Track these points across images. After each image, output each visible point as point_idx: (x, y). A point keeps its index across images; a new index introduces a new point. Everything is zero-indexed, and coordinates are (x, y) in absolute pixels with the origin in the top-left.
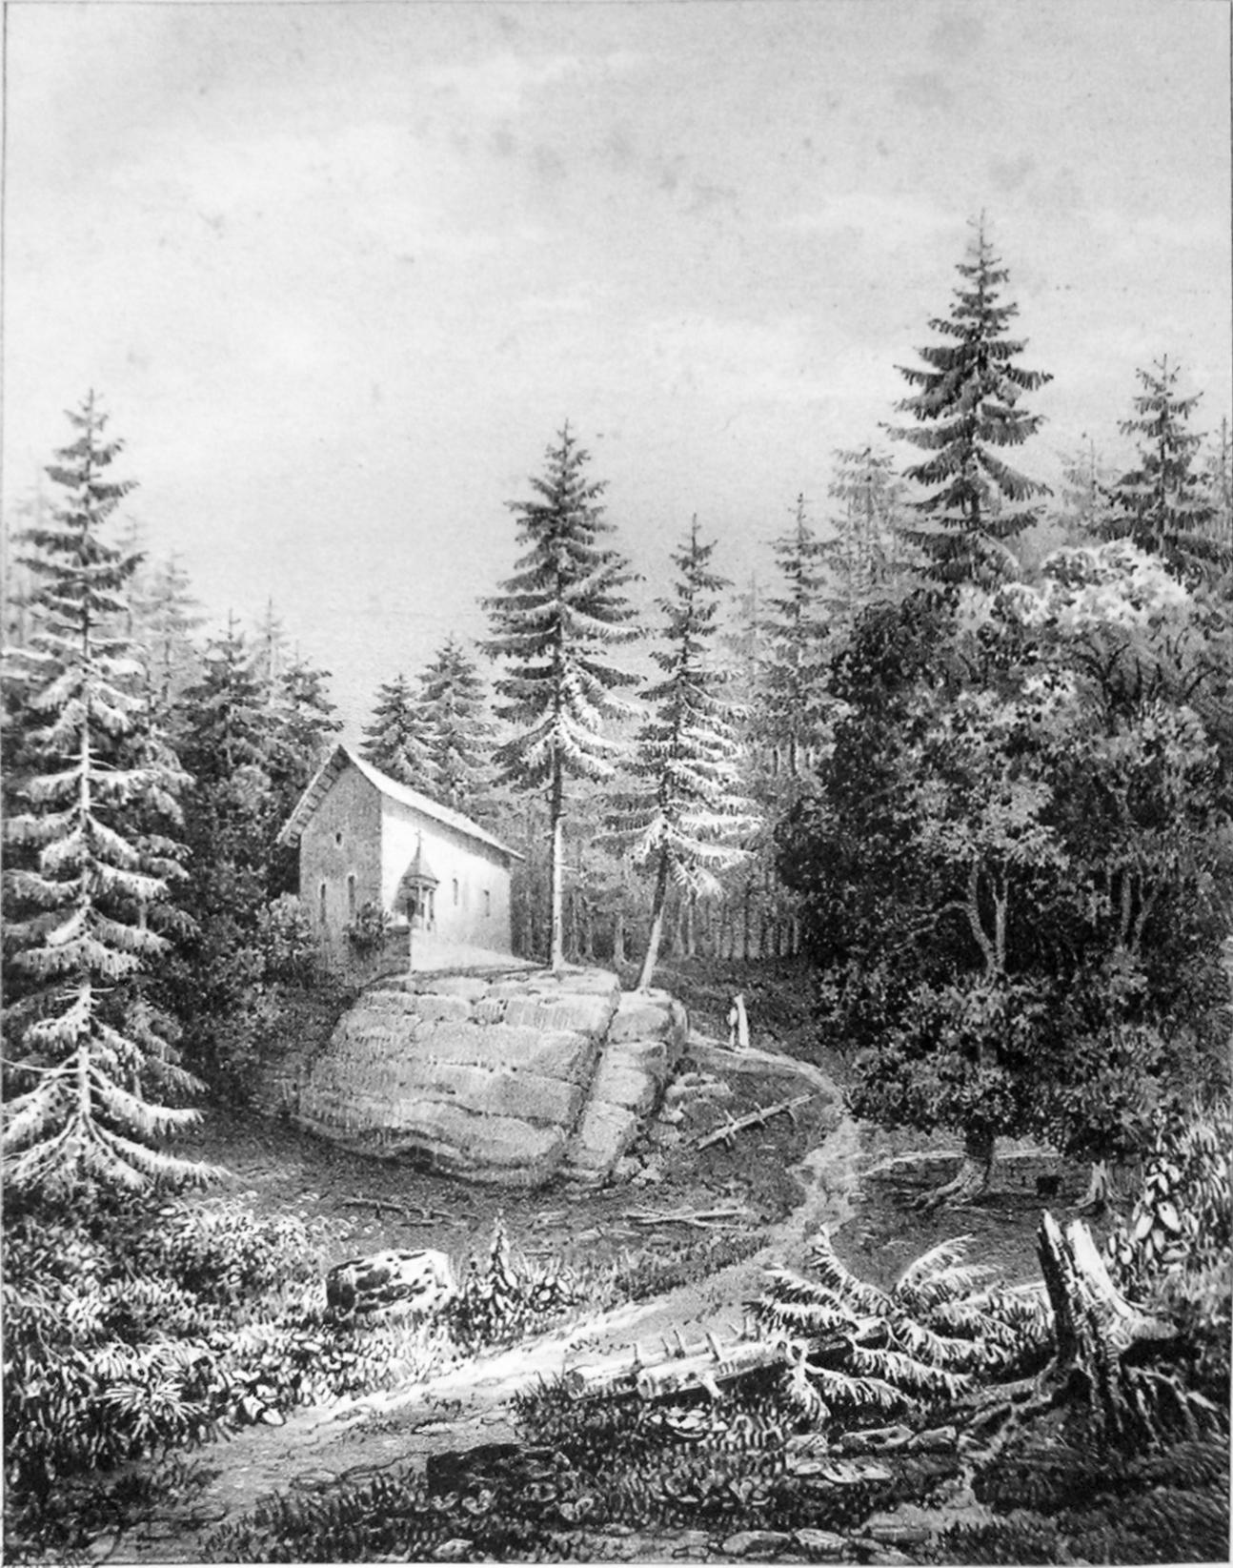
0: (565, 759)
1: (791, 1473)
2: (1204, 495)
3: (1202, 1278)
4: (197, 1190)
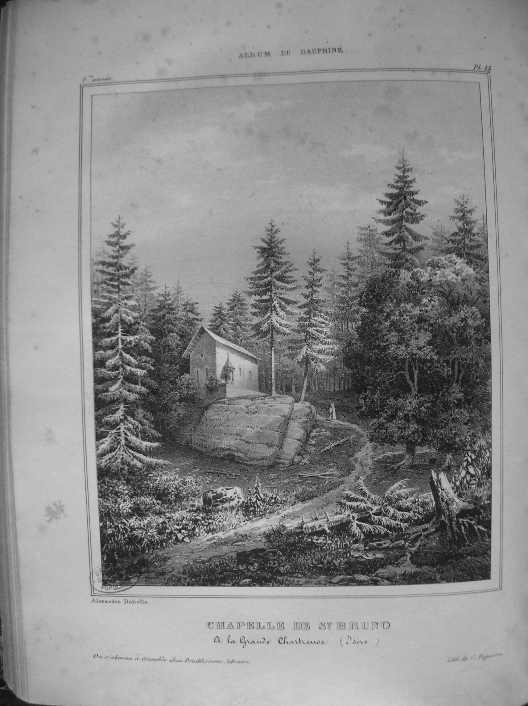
0: (274, 328)
1: (352, 556)
2: (478, 239)
3: (482, 489)
4: (160, 468)
